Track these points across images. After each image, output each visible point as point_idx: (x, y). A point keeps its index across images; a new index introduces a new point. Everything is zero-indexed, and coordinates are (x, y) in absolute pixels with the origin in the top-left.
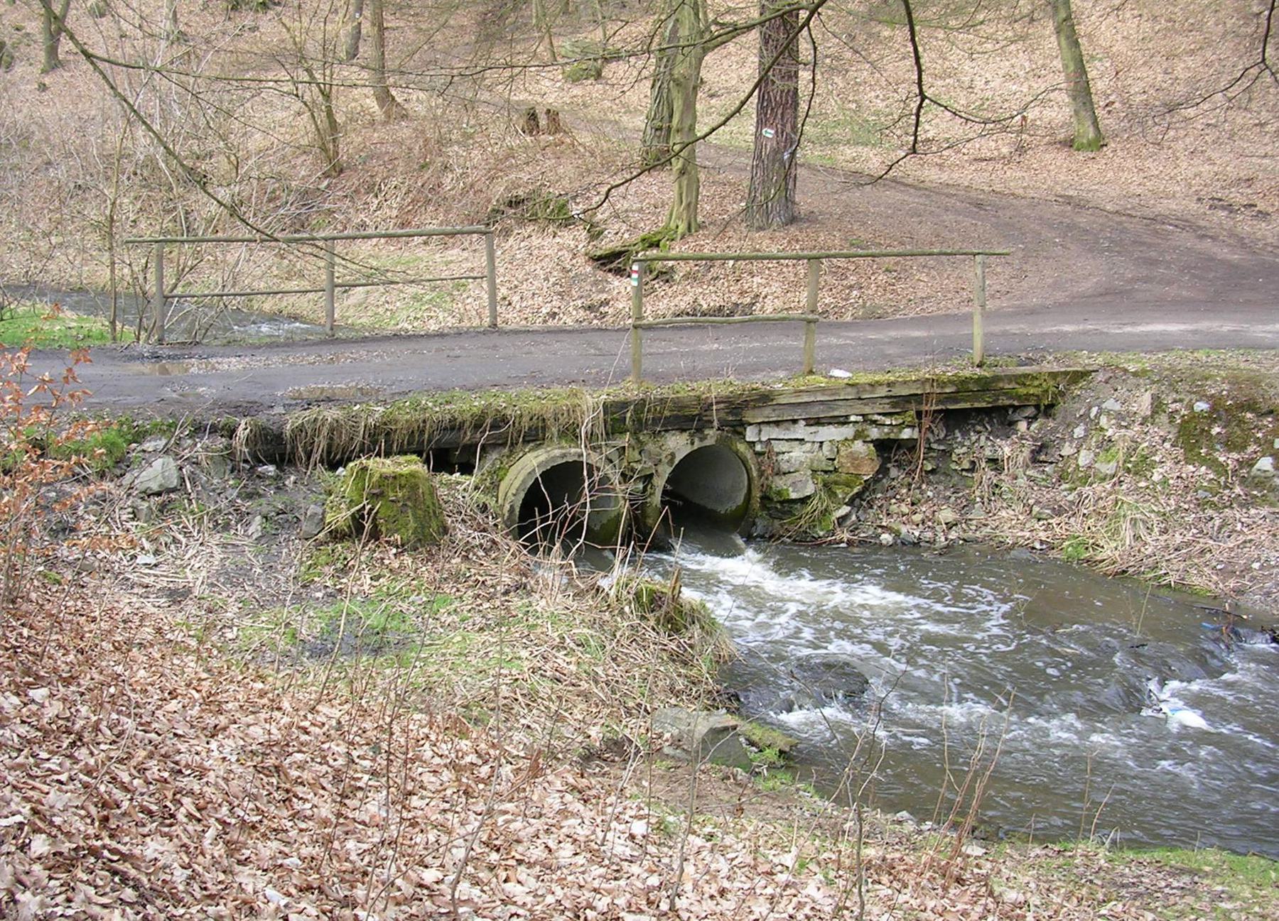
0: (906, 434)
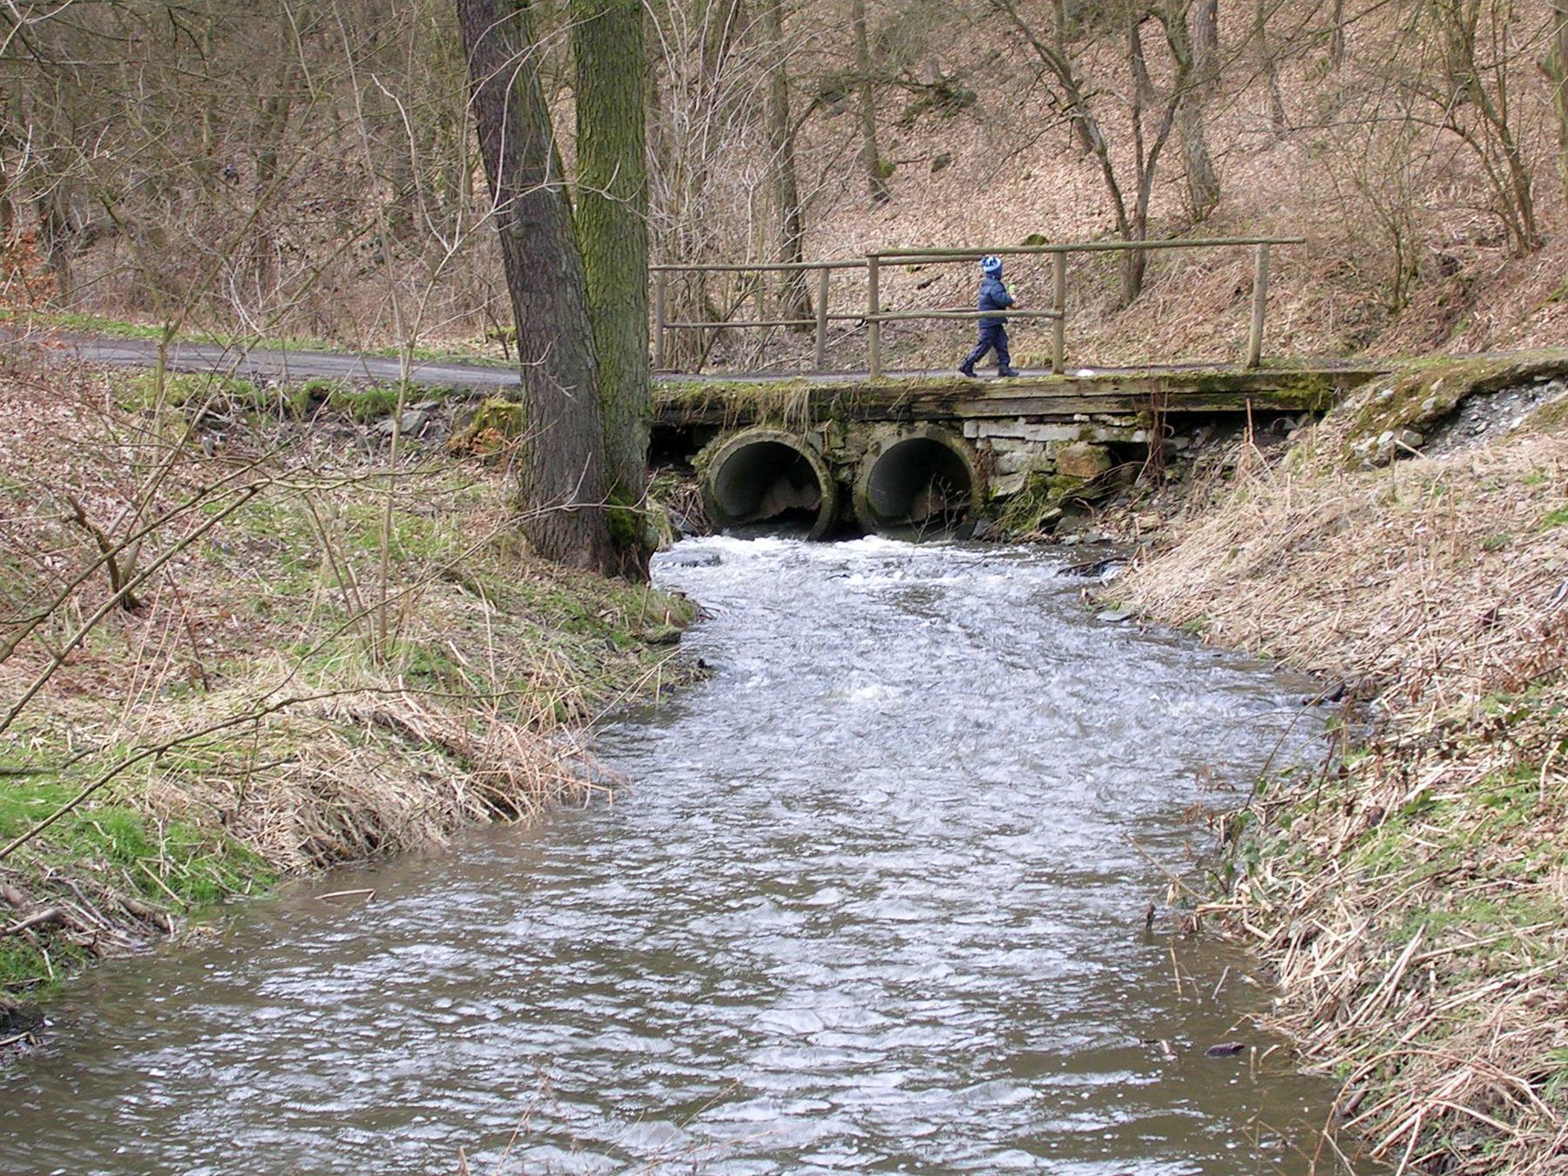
0: (1139, 437)
